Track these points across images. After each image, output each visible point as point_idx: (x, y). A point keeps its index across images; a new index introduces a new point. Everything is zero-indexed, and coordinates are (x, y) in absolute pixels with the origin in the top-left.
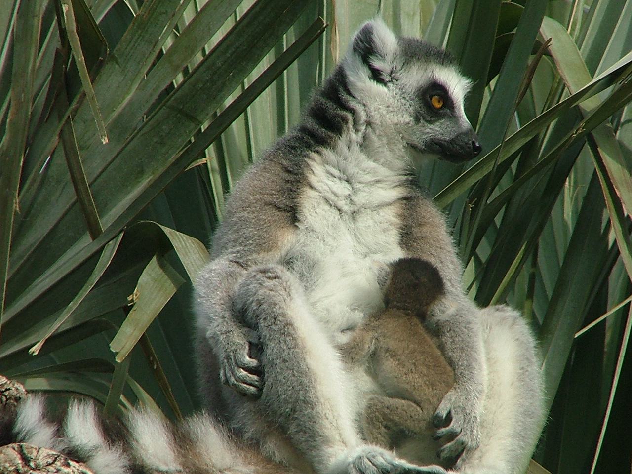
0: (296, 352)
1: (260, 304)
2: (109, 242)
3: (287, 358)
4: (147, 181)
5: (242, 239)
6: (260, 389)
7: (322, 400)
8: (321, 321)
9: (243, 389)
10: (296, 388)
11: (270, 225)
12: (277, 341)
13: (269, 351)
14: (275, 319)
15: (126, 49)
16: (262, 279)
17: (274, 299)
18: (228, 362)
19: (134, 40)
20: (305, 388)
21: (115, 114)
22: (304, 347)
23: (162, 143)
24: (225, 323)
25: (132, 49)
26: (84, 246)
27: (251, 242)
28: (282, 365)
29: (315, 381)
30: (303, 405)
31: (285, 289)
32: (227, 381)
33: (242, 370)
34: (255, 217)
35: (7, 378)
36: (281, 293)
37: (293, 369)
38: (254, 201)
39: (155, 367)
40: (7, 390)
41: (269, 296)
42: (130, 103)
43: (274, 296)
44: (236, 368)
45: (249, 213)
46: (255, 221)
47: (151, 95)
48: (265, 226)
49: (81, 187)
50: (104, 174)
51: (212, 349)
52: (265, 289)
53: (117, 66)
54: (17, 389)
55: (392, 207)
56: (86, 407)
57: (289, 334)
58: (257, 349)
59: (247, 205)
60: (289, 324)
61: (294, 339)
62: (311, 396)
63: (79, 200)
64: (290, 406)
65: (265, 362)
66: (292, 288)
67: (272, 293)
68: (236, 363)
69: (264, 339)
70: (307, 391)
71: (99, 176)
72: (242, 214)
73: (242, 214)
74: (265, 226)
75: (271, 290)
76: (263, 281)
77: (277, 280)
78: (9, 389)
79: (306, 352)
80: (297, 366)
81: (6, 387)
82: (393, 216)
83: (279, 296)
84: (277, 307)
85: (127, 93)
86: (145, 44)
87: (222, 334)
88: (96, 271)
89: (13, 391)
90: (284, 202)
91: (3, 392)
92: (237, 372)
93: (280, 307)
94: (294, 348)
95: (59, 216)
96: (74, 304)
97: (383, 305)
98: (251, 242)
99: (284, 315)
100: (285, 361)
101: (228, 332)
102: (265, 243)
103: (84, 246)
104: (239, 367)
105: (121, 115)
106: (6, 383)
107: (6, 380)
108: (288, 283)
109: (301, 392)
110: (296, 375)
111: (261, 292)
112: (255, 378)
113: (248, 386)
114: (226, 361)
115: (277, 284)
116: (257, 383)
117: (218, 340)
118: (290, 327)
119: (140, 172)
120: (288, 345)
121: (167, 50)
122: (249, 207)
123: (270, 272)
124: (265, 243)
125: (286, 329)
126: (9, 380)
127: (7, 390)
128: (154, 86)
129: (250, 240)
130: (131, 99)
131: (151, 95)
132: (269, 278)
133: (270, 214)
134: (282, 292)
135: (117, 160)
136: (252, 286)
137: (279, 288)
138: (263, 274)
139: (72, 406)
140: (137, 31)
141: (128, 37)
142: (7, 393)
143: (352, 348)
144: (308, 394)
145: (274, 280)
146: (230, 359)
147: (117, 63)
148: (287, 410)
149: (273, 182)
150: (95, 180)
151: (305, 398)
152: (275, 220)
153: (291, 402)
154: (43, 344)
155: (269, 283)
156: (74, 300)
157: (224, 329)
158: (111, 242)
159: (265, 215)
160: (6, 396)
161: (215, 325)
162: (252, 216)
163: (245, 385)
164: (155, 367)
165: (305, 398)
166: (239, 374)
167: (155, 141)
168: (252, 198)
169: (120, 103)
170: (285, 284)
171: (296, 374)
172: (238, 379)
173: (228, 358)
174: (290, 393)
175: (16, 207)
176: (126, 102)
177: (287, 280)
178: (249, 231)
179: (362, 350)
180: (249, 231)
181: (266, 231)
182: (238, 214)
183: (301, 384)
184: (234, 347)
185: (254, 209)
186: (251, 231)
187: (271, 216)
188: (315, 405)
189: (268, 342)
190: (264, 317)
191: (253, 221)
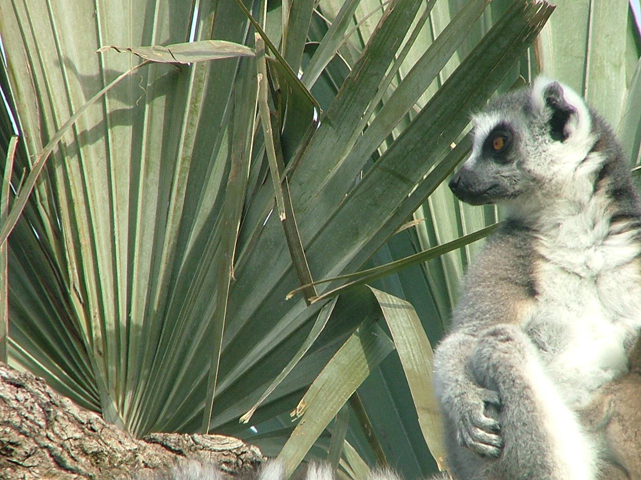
0: (535, 415)
1: (495, 367)
2: (324, 306)
3: (526, 421)
4: (363, 242)
5: (478, 313)
6: (501, 447)
7: (559, 465)
8: (577, 411)
9: (482, 450)
10: (534, 453)
11: (508, 298)
12: (517, 404)
13: (509, 414)
14: (514, 381)
15: (339, 110)
16: (494, 342)
17: (510, 361)
18: (464, 423)
19: (347, 101)
20: (543, 453)
21: (330, 176)
22: (542, 411)
23: (376, 205)
24: (458, 386)
25: (345, 110)
26: (299, 313)
27: (488, 316)
28: (522, 428)
29: (553, 446)
30: (540, 470)
31: (519, 351)
32: (464, 443)
33: (478, 430)
34: (491, 291)
35: (243, 441)
36: (516, 355)
37: (532, 433)
38: (489, 276)
39: (370, 434)
40: (242, 453)
41: (504, 358)
42: (345, 164)
43: (510, 358)
44: (473, 428)
45: (484, 287)
46: (492, 295)
47: (364, 156)
48: (502, 299)
49: (296, 252)
50: (320, 237)
51: (448, 414)
52: (499, 351)
53: (330, 128)
54: (253, 452)
55: (633, 265)
56: (324, 470)
57: (528, 398)
58: (496, 408)
59: (482, 280)
60: (526, 387)
61: (532, 402)
62: (548, 461)
63: (295, 265)
64: (528, 471)
65: (505, 422)
66: (526, 349)
67: (507, 355)
68: (472, 423)
69: (506, 400)
70: (544, 456)
71: (314, 239)
72: (478, 289)
73: (478, 289)
74: (502, 299)
75: (506, 353)
76: (496, 344)
77: (510, 342)
78: (245, 452)
79: (544, 416)
80: (535, 430)
81: (242, 450)
82: (637, 274)
83: (515, 358)
84: (514, 369)
85: (343, 155)
86: (357, 105)
87: (456, 397)
88: (310, 336)
89: (249, 455)
90: (521, 278)
91: (239, 455)
92: (474, 432)
93: (517, 370)
94: (532, 412)
95: (277, 280)
96: (287, 370)
97: (626, 369)
98: (488, 316)
99: (521, 378)
100: (524, 424)
101: (463, 394)
102: (503, 316)
103: (299, 313)
104: (476, 427)
105: (335, 178)
106: (242, 446)
107: (242, 443)
108: (522, 345)
109: (539, 457)
110: (535, 439)
111: (495, 356)
112: (494, 436)
113: (486, 446)
114: (461, 422)
115: (511, 346)
116: (494, 442)
117: (453, 403)
118: (527, 390)
119: (355, 234)
120: (527, 408)
121: (352, 67)
122: (484, 281)
123: (502, 334)
124: (503, 316)
125: (525, 393)
126: (245, 443)
127: (242, 453)
128: (367, 147)
129: (487, 314)
130: (346, 160)
131: (364, 156)
132: (502, 341)
133: (503, 289)
134: (517, 354)
135: (333, 223)
136: (485, 350)
137: (514, 350)
138: (495, 338)
139: (311, 468)
140: (348, 93)
141: (340, 99)
142: (243, 457)
143: (591, 410)
144: (545, 459)
145: (507, 342)
146: (466, 420)
147: (330, 124)
148: (525, 475)
149: (505, 257)
150: (311, 244)
151: (542, 463)
152: (513, 294)
153: (529, 467)
154: (254, 412)
155: (503, 346)
156: (288, 365)
157: (458, 392)
158: (326, 306)
159: (501, 288)
160: (242, 460)
161: (450, 389)
162: (488, 290)
163: (483, 445)
164: (370, 434)
165: (542, 463)
166: (476, 434)
167: (369, 202)
168: (486, 273)
169: (335, 165)
170: (518, 346)
171: (535, 439)
172: (475, 439)
173: (463, 419)
174: (528, 457)
175: (231, 275)
176: (340, 163)
177: (520, 341)
178: (486, 305)
179: (602, 413)
180: (486, 305)
181: (503, 305)
182: (473, 290)
183: (539, 448)
184: (469, 407)
185: (489, 283)
186: (487, 305)
187: (508, 290)
188: (553, 469)
189: (510, 405)
190: (502, 380)
191: (489, 295)
